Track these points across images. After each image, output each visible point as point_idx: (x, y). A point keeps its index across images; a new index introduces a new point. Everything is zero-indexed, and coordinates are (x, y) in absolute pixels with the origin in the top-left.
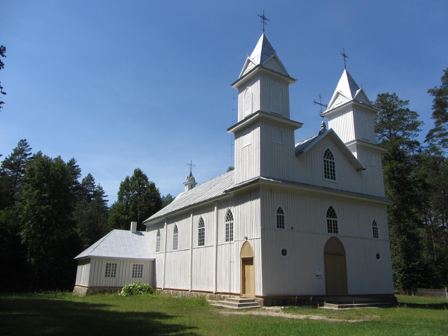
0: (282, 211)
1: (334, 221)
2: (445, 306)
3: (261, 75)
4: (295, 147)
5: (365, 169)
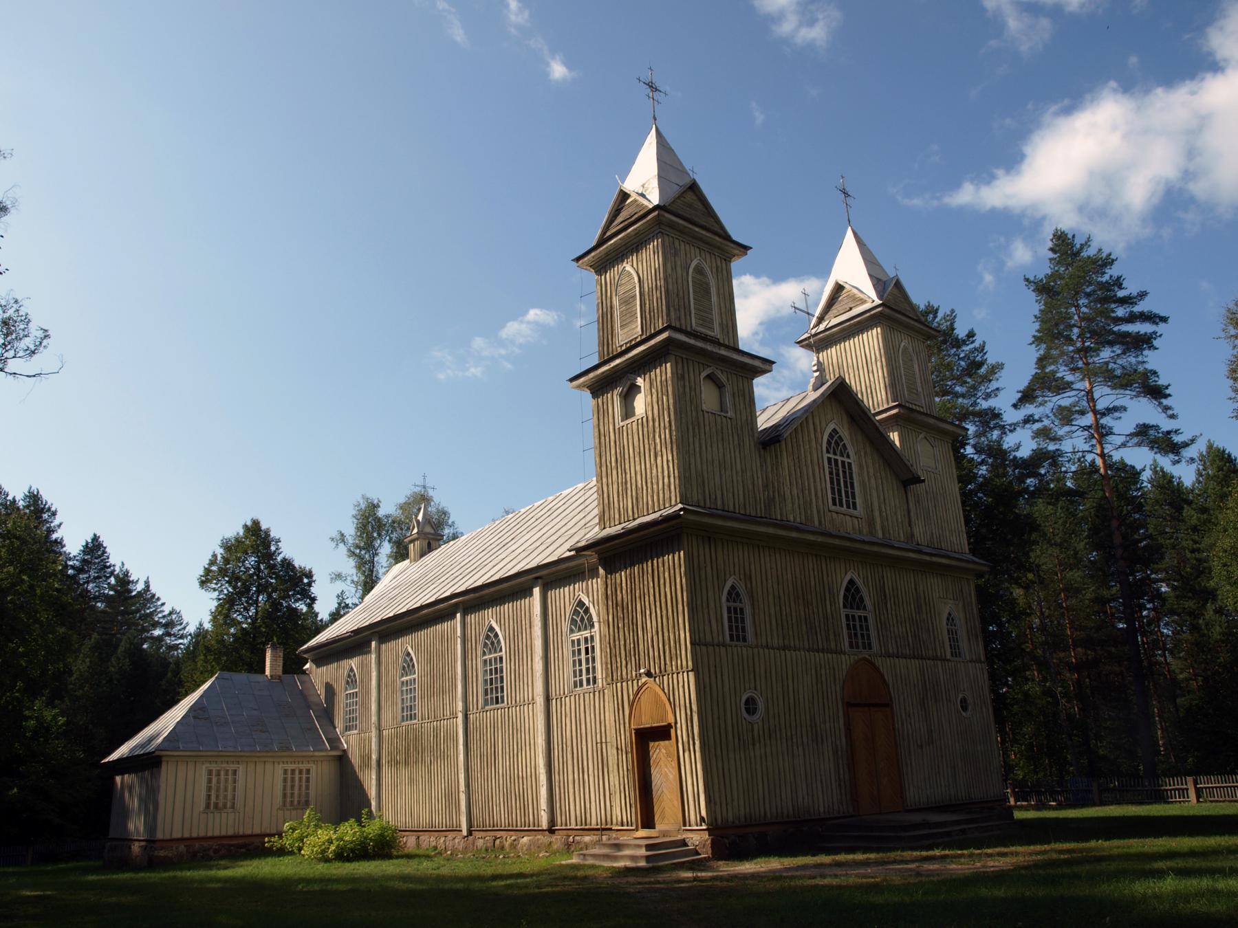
0: (738, 595)
1: (860, 617)
2: (136, 848)
3: (662, 233)
4: (765, 421)
5: (923, 481)
